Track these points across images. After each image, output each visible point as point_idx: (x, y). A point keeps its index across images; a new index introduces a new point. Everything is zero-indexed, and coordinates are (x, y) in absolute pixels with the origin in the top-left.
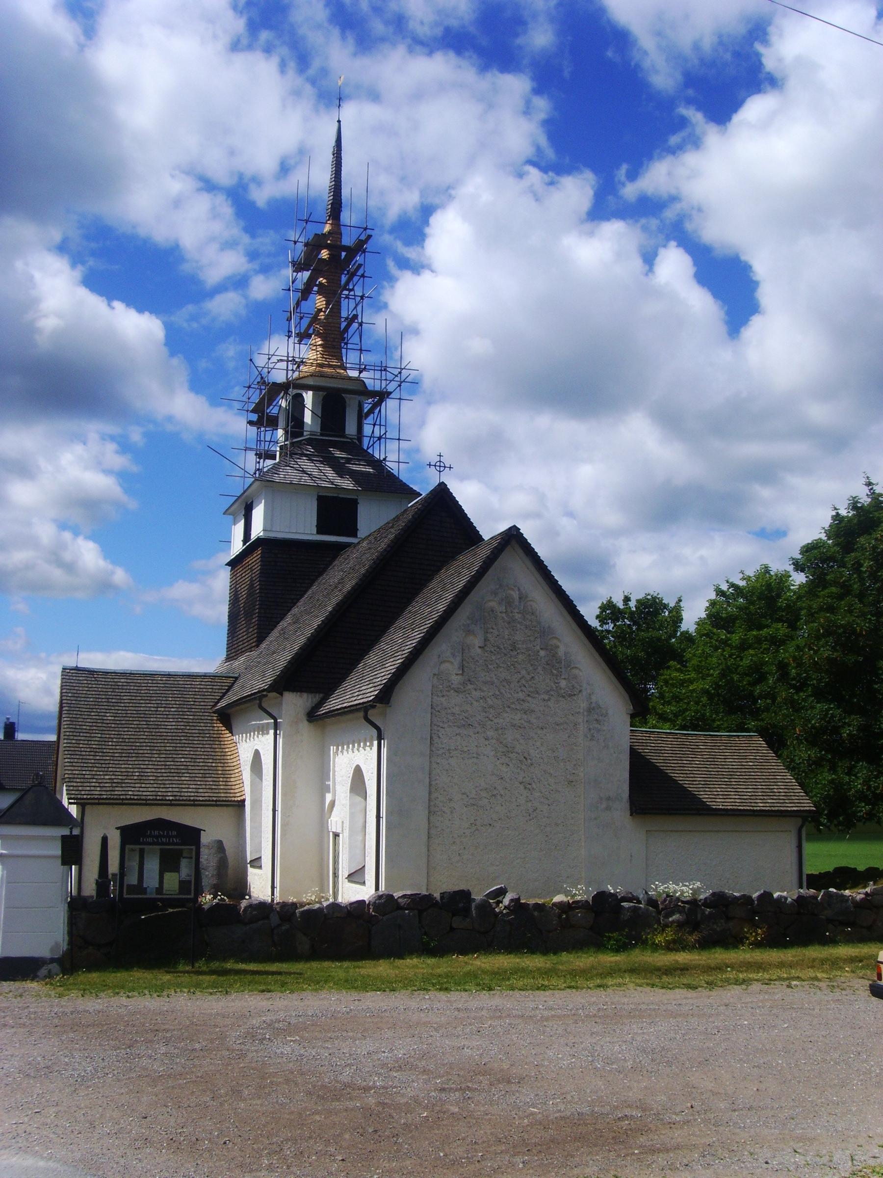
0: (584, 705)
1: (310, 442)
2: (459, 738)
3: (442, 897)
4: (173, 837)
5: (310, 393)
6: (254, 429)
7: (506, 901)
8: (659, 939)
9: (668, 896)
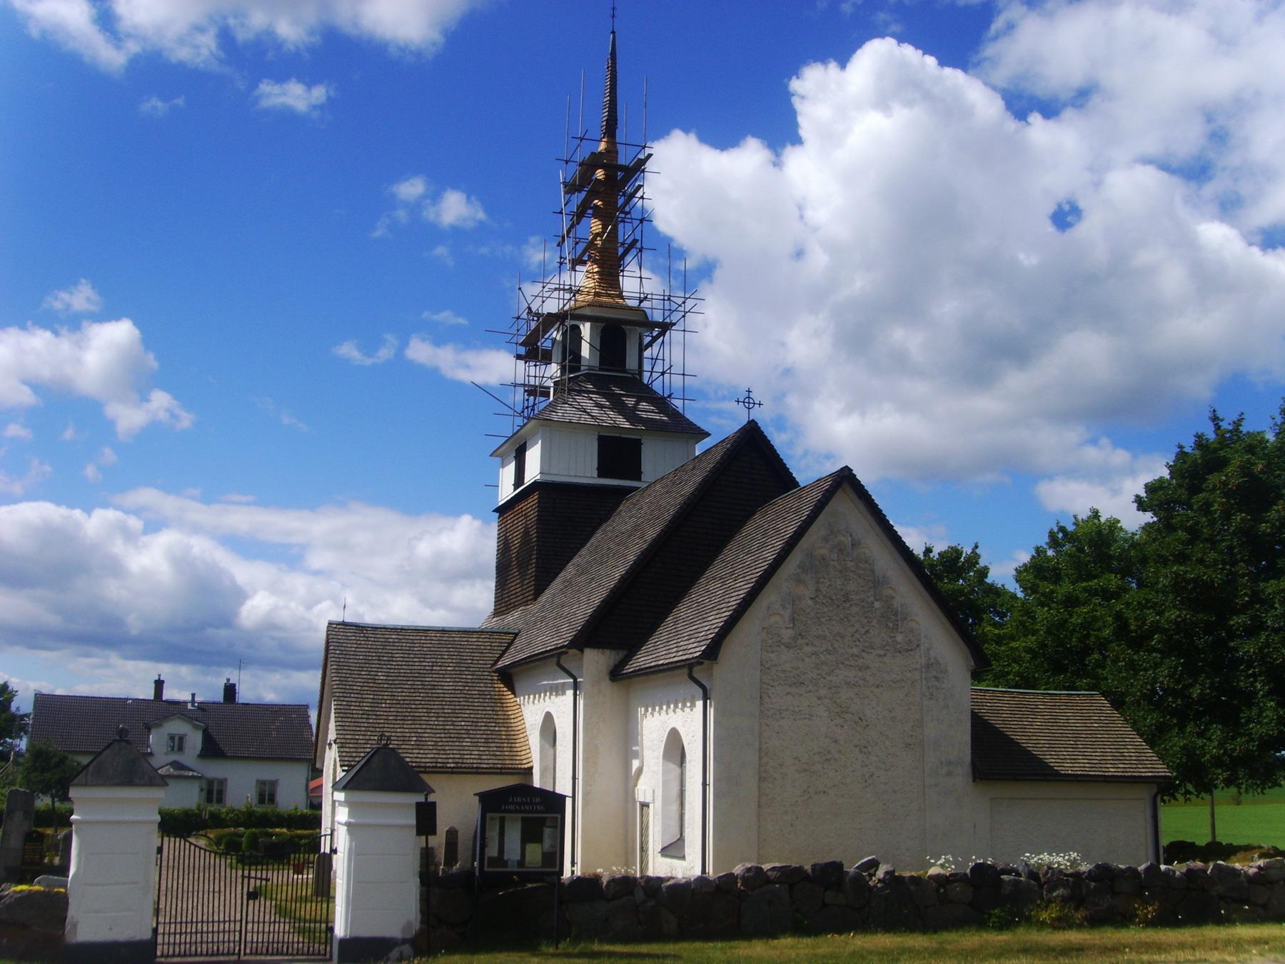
0: (923, 661)
1: (589, 377)
2: (789, 697)
5: (588, 325)
6: (521, 363)
7: (880, 873)
8: (1044, 916)
9: (1049, 868)
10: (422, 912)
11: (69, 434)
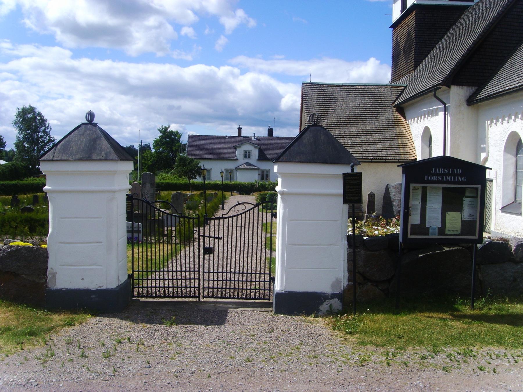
3: (195, 176)
4: (458, 175)
10: (349, 271)
11: (207, 32)
